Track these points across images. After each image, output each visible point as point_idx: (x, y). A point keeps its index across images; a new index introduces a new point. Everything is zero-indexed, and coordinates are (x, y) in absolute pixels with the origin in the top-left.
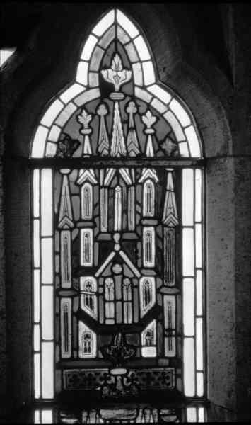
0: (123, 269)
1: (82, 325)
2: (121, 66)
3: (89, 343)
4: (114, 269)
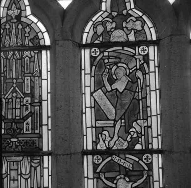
2: (15, 9)
3: (29, 127)
4: (16, 94)
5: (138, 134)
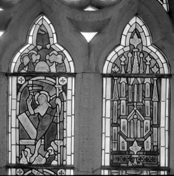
0: (137, 117)
1: (121, 138)
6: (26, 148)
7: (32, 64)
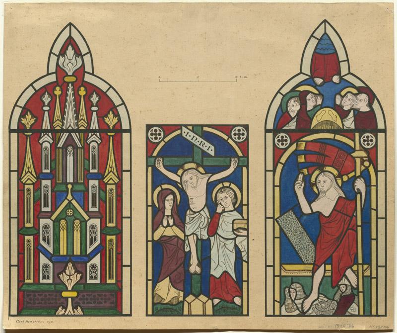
5: (353, 290)
6: (292, 283)
7: (305, 117)
